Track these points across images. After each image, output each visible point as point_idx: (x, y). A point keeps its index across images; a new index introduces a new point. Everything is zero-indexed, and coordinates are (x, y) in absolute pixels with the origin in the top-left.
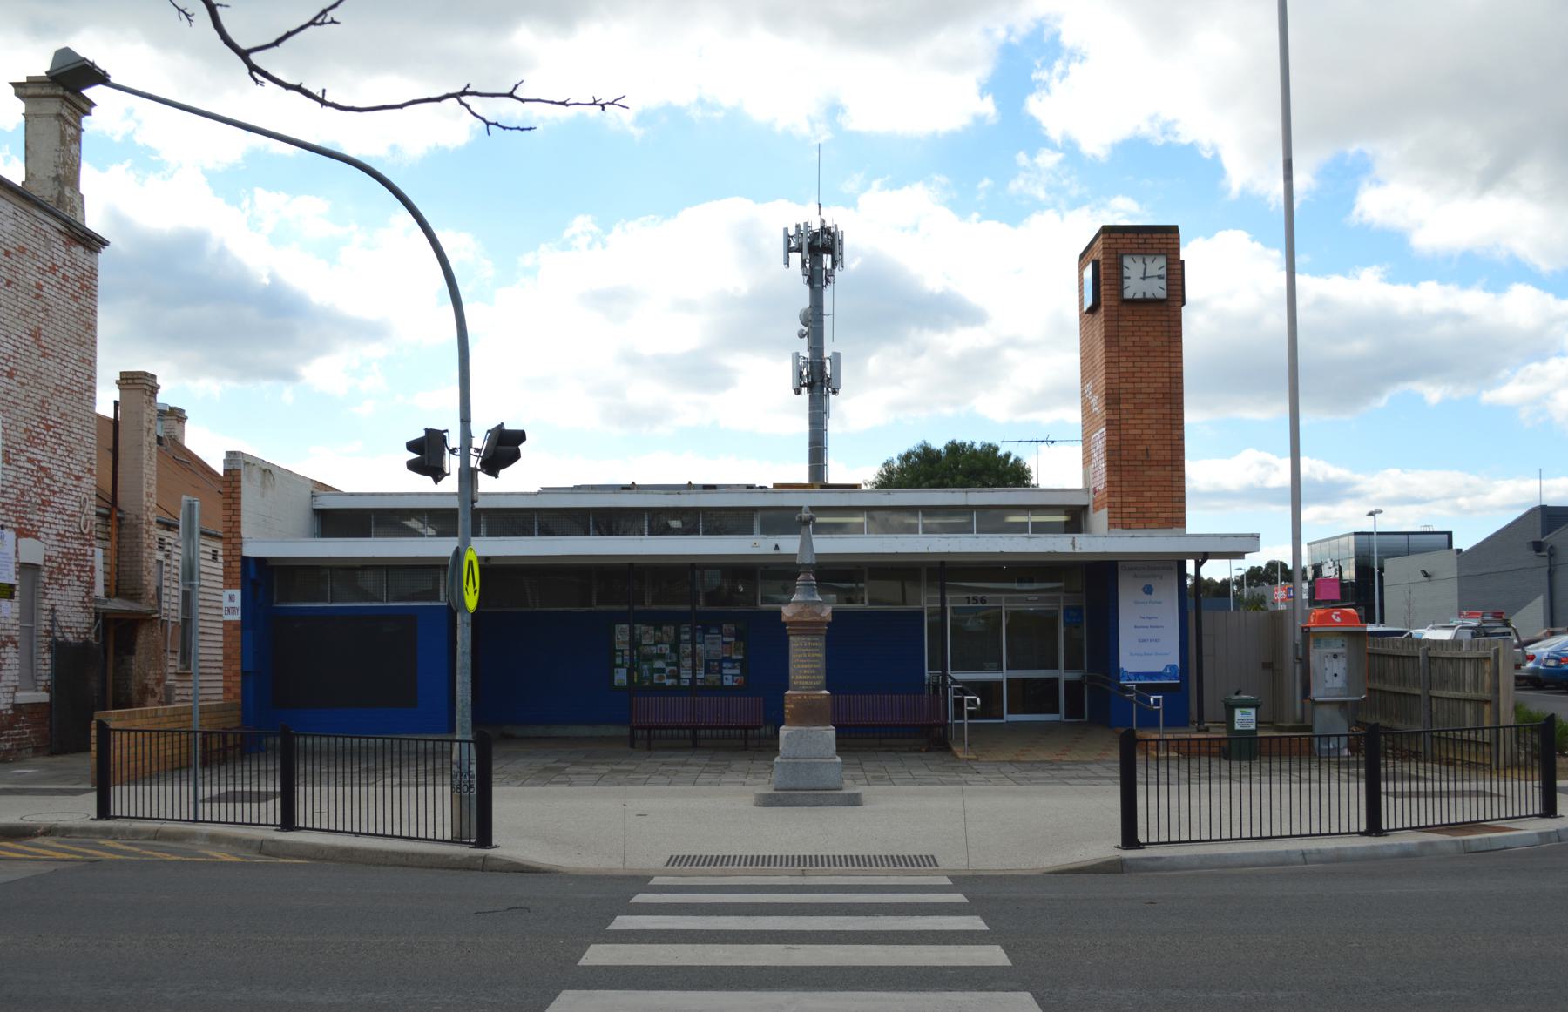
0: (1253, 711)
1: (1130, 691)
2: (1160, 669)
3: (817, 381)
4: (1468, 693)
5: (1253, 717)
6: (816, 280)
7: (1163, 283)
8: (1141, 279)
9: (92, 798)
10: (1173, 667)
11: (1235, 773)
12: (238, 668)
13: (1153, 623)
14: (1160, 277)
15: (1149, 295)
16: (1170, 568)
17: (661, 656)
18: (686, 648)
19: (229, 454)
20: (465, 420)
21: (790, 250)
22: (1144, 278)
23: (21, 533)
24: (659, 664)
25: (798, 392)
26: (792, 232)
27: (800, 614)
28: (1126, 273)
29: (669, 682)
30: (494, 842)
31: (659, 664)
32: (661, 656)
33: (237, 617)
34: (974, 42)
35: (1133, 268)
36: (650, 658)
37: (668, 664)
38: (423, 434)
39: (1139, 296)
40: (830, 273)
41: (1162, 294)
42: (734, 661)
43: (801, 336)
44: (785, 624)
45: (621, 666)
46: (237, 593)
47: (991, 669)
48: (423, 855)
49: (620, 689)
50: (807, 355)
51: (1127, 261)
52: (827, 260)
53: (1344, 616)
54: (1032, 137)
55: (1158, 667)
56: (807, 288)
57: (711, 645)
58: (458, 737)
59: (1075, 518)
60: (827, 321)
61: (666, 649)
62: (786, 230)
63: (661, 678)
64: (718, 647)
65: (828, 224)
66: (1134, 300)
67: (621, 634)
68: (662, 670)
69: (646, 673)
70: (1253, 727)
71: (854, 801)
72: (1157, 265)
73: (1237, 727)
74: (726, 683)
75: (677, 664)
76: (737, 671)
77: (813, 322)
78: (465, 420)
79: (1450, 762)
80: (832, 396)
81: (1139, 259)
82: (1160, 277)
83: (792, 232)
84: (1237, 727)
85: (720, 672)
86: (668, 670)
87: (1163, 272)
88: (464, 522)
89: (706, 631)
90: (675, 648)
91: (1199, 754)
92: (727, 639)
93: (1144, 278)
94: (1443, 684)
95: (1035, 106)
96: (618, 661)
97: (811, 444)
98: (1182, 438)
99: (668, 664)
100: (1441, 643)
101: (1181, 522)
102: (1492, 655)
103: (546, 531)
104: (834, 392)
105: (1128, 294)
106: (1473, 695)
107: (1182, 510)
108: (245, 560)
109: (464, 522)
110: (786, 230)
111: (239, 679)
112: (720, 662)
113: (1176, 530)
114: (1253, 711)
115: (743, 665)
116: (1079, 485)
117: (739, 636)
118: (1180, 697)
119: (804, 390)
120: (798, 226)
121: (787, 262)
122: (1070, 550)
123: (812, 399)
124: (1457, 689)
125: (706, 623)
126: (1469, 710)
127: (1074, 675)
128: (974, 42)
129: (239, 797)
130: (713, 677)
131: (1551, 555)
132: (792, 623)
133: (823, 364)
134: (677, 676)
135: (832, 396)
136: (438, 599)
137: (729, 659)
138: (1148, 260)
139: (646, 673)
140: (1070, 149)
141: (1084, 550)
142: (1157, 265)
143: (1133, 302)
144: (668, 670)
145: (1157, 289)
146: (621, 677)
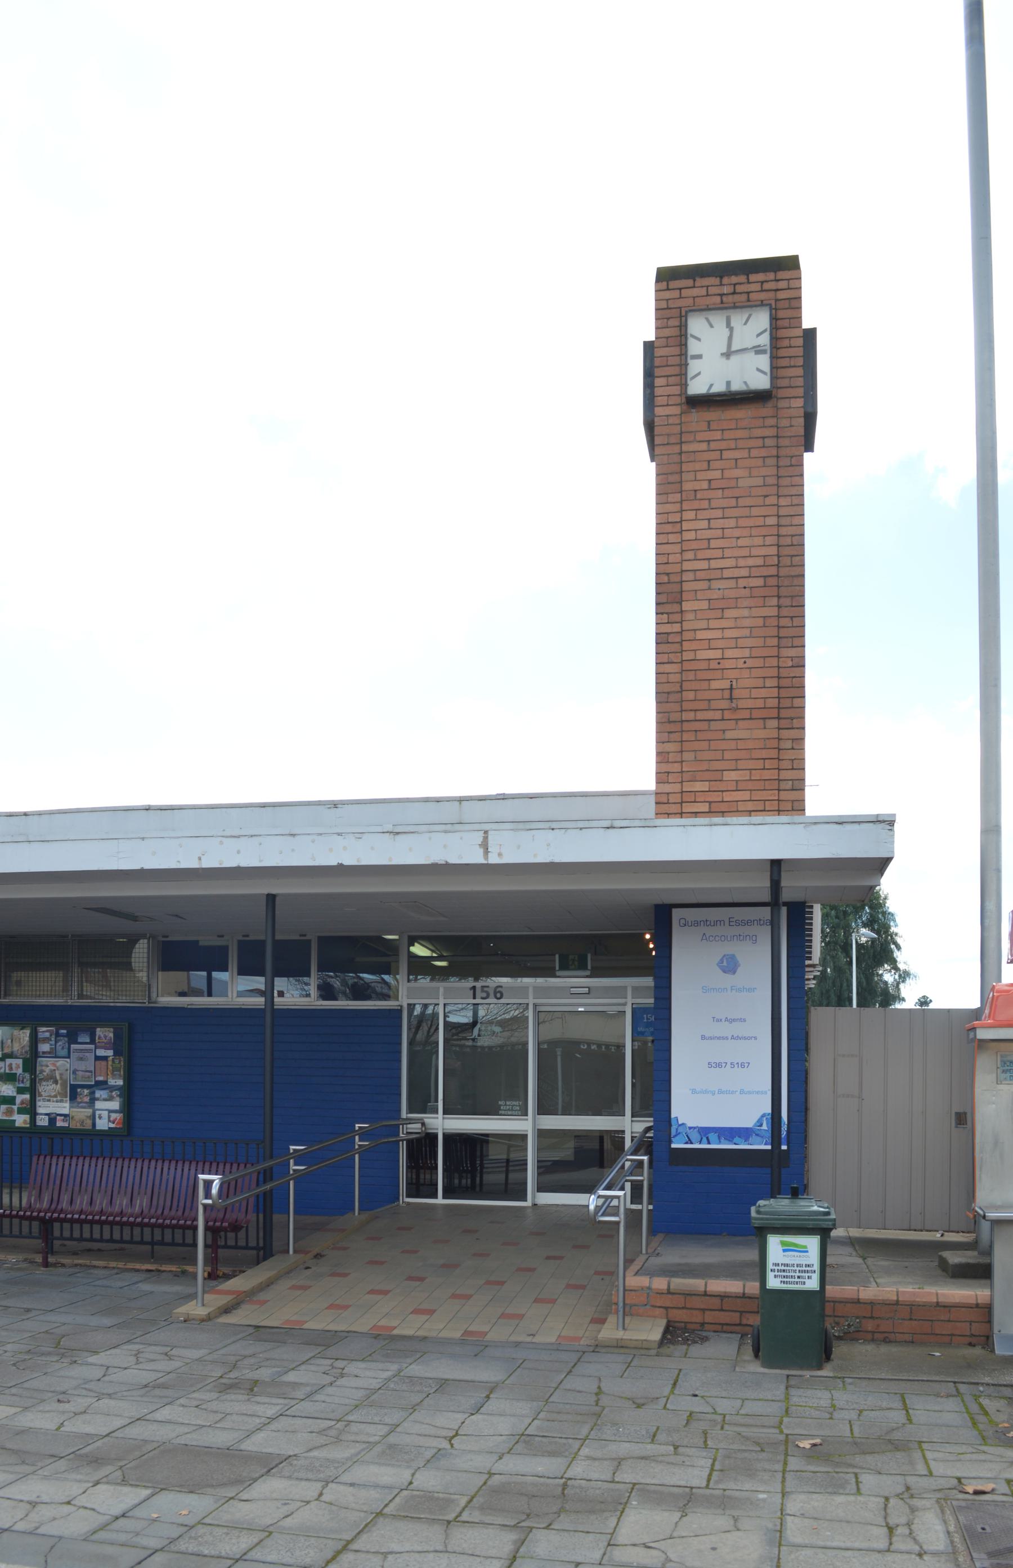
0: (812, 1243)
5: (813, 1257)
7: (764, 361)
8: (726, 356)
9: (510, 1181)
13: (737, 1029)
14: (758, 350)
15: (737, 386)
19: (688, 290)
22: (728, 355)
23: (653, 1041)
28: (694, 347)
29: (21, 1120)
39: (719, 388)
41: (762, 382)
42: (112, 1088)
47: (511, 1113)
64: (90, 1064)
72: (753, 328)
81: (718, 320)
87: (765, 340)
89: (72, 1039)
92: (101, 1052)
93: (728, 355)
98: (800, 664)
99: (21, 1091)
105: (697, 387)
114: (812, 1243)
115: (129, 1096)
118: (716, 1193)
122: (475, 857)
130: (81, 1113)
134: (31, 1109)
137: (102, 1085)
138: (737, 319)
141: (511, 857)
142: (753, 328)
145: (752, 373)
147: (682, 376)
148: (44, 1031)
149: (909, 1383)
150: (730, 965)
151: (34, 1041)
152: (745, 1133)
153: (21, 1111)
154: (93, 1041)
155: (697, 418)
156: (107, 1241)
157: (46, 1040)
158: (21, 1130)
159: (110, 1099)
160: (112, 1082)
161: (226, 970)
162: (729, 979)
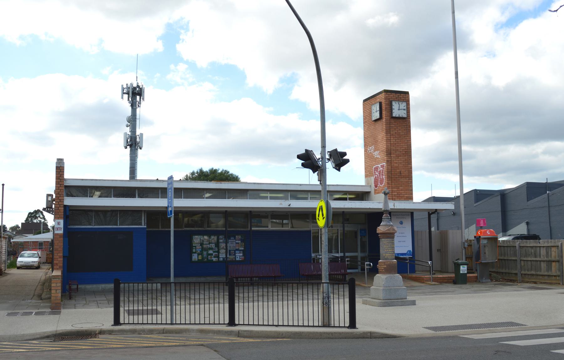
0: (466, 266)
1: (407, 260)
2: (406, 252)
3: (133, 143)
4: (542, 258)
5: (466, 268)
6: (134, 105)
10: (410, 251)
11: (265, 294)
12: (62, 254)
14: (404, 110)
15: (401, 116)
16: (409, 215)
17: (212, 249)
18: (223, 245)
19: (58, 160)
20: (324, 146)
21: (124, 93)
22: (399, 109)
24: (211, 252)
25: (126, 148)
26: (125, 86)
27: (388, 230)
28: (393, 107)
29: (214, 259)
30: (357, 326)
31: (211, 252)
32: (212, 249)
33: (61, 232)
34: (157, 23)
35: (395, 105)
36: (207, 250)
37: (214, 252)
38: (304, 152)
39: (397, 116)
40: (140, 103)
41: (405, 116)
43: (127, 126)
44: (378, 234)
45: (195, 253)
46: (62, 221)
48: (340, 333)
49: (195, 262)
50: (130, 133)
51: (394, 103)
52: (138, 97)
53: (490, 232)
54: (178, 60)
55: (405, 251)
56: (130, 108)
57: (233, 244)
58: (323, 281)
59: (362, 196)
60: (138, 121)
61: (213, 246)
62: (122, 86)
63: (211, 258)
64: (235, 245)
65: (140, 85)
66: (390, 117)
67: (197, 239)
68: (212, 254)
69: (205, 255)
70: (466, 272)
71: (413, 303)
72: (403, 105)
73: (461, 272)
74: (237, 259)
75: (218, 252)
76: (241, 255)
77: (132, 121)
78: (324, 146)
79: (551, 284)
80: (139, 150)
81: (397, 102)
82: (404, 110)
83: (125, 86)
84: (461, 272)
85: (235, 255)
86: (214, 254)
88: (171, 193)
90: (217, 244)
91: (244, 286)
92: (237, 242)
93: (399, 109)
94: (526, 256)
95: (180, 47)
96: (194, 251)
97: (131, 168)
99: (214, 252)
100: (507, 241)
101: (411, 198)
102: (560, 245)
103: (141, 196)
104: (140, 149)
105: (394, 115)
106: (546, 259)
107: (412, 194)
108: (65, 206)
109: (171, 193)
110: (122, 86)
111: (62, 259)
112: (235, 251)
113: (410, 201)
114: (466, 266)
116: (328, 183)
117: (242, 241)
119: (128, 147)
120: (127, 84)
121: (122, 98)
123: (131, 150)
124: (536, 257)
125: (228, 235)
126: (543, 265)
127: (363, 255)
128: (157, 23)
129: (150, 312)
130: (232, 257)
131: (438, 213)
132: (381, 233)
133: (135, 138)
134: (218, 257)
135: (139, 150)
136: (141, 225)
138: (400, 103)
139: (205, 255)
140: (192, 66)
141: (398, 208)
143: (396, 118)
144: (214, 254)
145: (403, 114)
146: (195, 257)
147: (391, 112)
148: (221, 237)
149: (399, 298)
150: (401, 223)
151: (218, 239)
152: (163, 181)
153: (214, 257)
154: (235, 239)
155: (392, 121)
156: (276, 326)
157: (221, 239)
158: (215, 262)
159: (240, 253)
160: (240, 249)
161: (175, 189)
162: (401, 226)
